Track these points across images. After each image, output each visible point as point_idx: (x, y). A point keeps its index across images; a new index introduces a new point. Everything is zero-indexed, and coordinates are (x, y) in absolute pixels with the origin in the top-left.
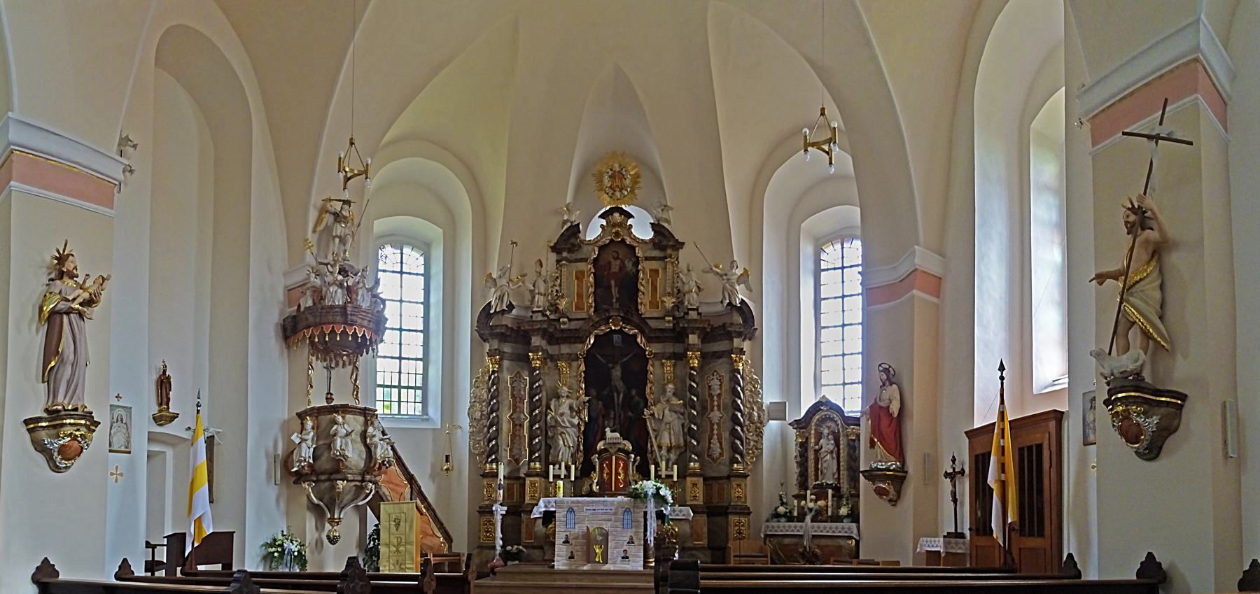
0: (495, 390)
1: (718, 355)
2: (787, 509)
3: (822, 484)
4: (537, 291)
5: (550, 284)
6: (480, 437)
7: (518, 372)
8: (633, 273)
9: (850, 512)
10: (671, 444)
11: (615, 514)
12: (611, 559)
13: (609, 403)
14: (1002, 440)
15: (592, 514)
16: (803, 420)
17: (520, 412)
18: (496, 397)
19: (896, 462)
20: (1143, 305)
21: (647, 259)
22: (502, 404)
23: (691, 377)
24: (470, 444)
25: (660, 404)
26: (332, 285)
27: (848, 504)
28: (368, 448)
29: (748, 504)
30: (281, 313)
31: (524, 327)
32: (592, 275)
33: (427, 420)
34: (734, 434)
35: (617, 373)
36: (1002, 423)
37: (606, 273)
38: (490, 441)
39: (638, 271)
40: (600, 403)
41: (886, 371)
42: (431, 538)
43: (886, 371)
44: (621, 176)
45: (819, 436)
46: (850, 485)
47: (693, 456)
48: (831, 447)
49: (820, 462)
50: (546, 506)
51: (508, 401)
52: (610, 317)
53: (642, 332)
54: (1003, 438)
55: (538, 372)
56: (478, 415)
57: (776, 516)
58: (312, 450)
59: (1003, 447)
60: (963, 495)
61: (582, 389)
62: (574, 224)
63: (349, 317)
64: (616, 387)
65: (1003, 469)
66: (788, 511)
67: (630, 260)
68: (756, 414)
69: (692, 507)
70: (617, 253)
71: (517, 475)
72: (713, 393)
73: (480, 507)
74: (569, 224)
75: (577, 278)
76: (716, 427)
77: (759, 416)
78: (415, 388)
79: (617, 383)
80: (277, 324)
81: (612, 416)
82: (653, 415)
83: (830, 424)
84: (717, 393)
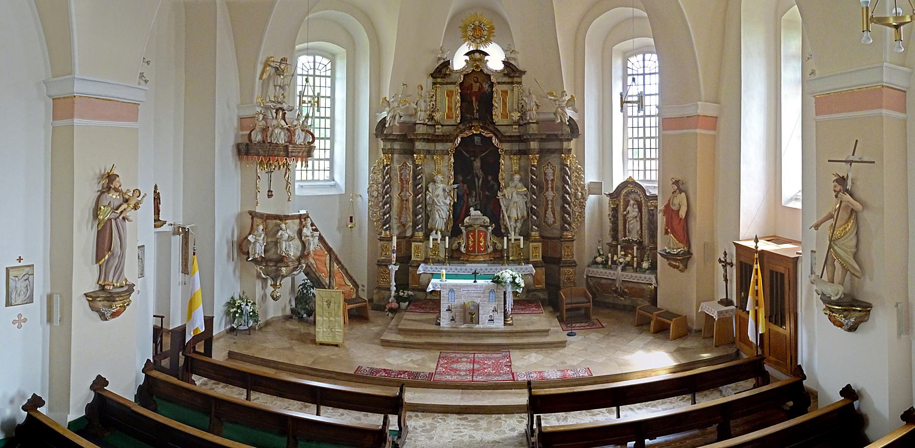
0: (388, 178)
1: (551, 151)
2: (603, 258)
3: (629, 240)
4: (419, 109)
5: (428, 100)
6: (377, 209)
7: (405, 163)
8: (489, 92)
9: (650, 266)
10: (518, 218)
11: (483, 293)
12: (481, 321)
13: (471, 186)
14: (756, 286)
15: (467, 293)
16: (614, 193)
17: (406, 191)
18: (389, 183)
19: (684, 248)
20: (845, 249)
21: (499, 83)
22: (393, 186)
23: (532, 172)
24: (369, 214)
25: (509, 188)
26: (277, 127)
27: (649, 260)
28: (303, 243)
29: (575, 259)
30: (236, 136)
31: (410, 136)
32: (459, 94)
33: (334, 186)
34: (563, 208)
35: (477, 164)
36: (756, 276)
37: (469, 92)
38: (385, 214)
39: (492, 92)
40: (465, 185)
41: (676, 183)
42: (344, 287)
43: (676, 183)
44: (481, 28)
45: (627, 204)
46: (650, 241)
47: (534, 227)
48: (635, 214)
49: (627, 224)
50: (433, 287)
51: (397, 184)
52: (473, 126)
53: (496, 136)
54: (757, 285)
55: (420, 168)
56: (375, 194)
57: (595, 263)
58: (263, 247)
59: (757, 291)
60: (732, 275)
61: (452, 175)
62: (446, 60)
63: (290, 154)
64: (477, 174)
65: (757, 303)
66: (604, 260)
67: (487, 83)
68: (580, 194)
69: (533, 263)
70: (478, 79)
71: (404, 235)
72: (548, 179)
73: (378, 261)
74: (442, 61)
75: (447, 95)
76: (550, 202)
77: (582, 194)
78: (325, 159)
79: (477, 171)
80: (233, 146)
81: (474, 195)
82: (504, 195)
83: (633, 196)
84: (551, 179)
